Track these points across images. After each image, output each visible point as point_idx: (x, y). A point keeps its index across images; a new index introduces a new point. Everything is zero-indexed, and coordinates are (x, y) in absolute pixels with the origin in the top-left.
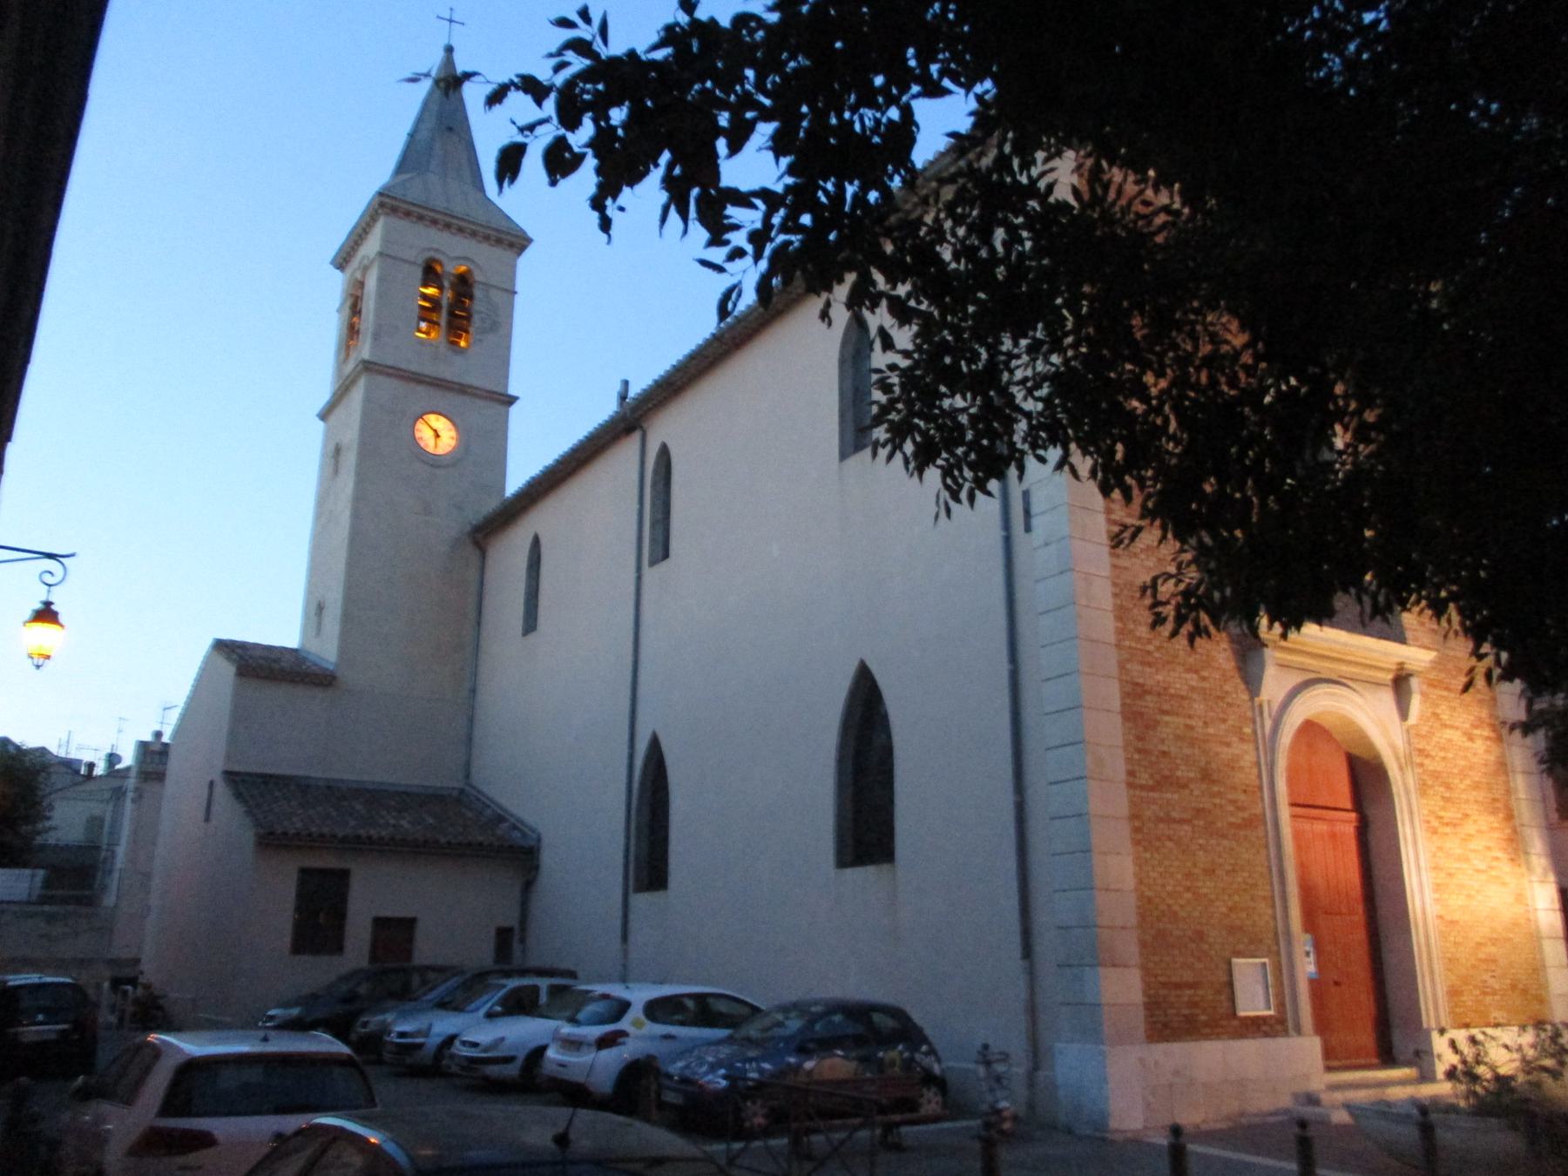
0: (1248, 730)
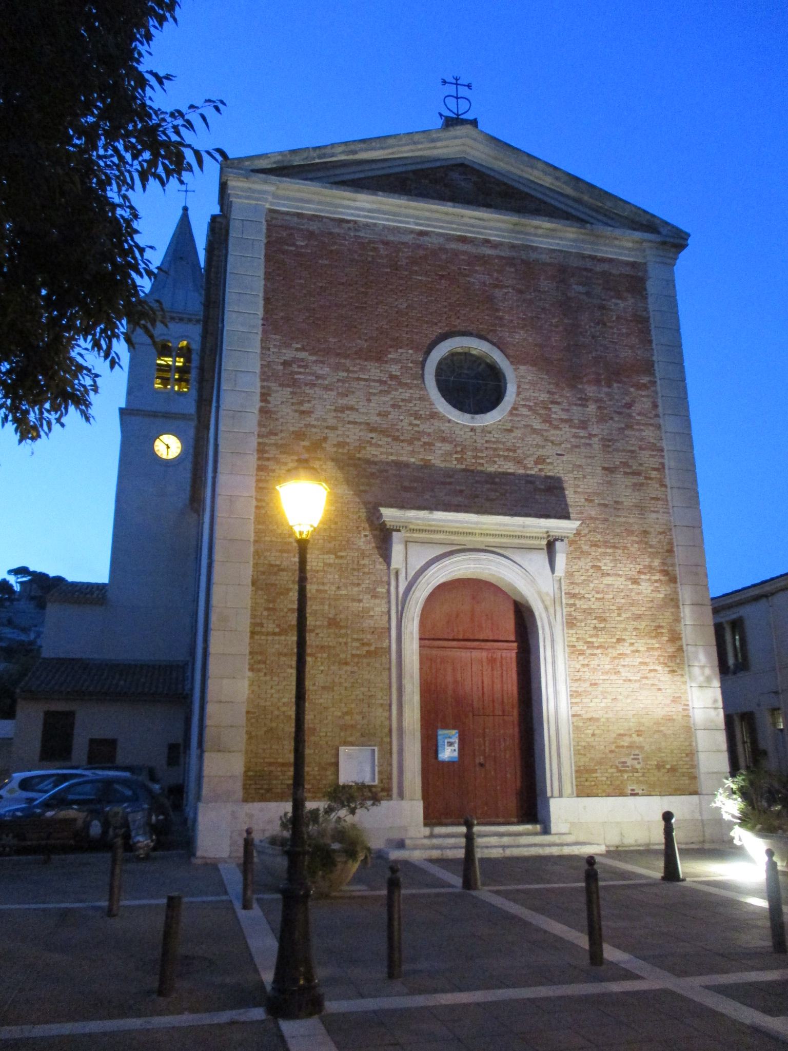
0: (382, 590)
